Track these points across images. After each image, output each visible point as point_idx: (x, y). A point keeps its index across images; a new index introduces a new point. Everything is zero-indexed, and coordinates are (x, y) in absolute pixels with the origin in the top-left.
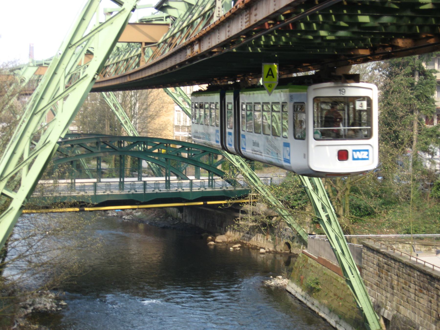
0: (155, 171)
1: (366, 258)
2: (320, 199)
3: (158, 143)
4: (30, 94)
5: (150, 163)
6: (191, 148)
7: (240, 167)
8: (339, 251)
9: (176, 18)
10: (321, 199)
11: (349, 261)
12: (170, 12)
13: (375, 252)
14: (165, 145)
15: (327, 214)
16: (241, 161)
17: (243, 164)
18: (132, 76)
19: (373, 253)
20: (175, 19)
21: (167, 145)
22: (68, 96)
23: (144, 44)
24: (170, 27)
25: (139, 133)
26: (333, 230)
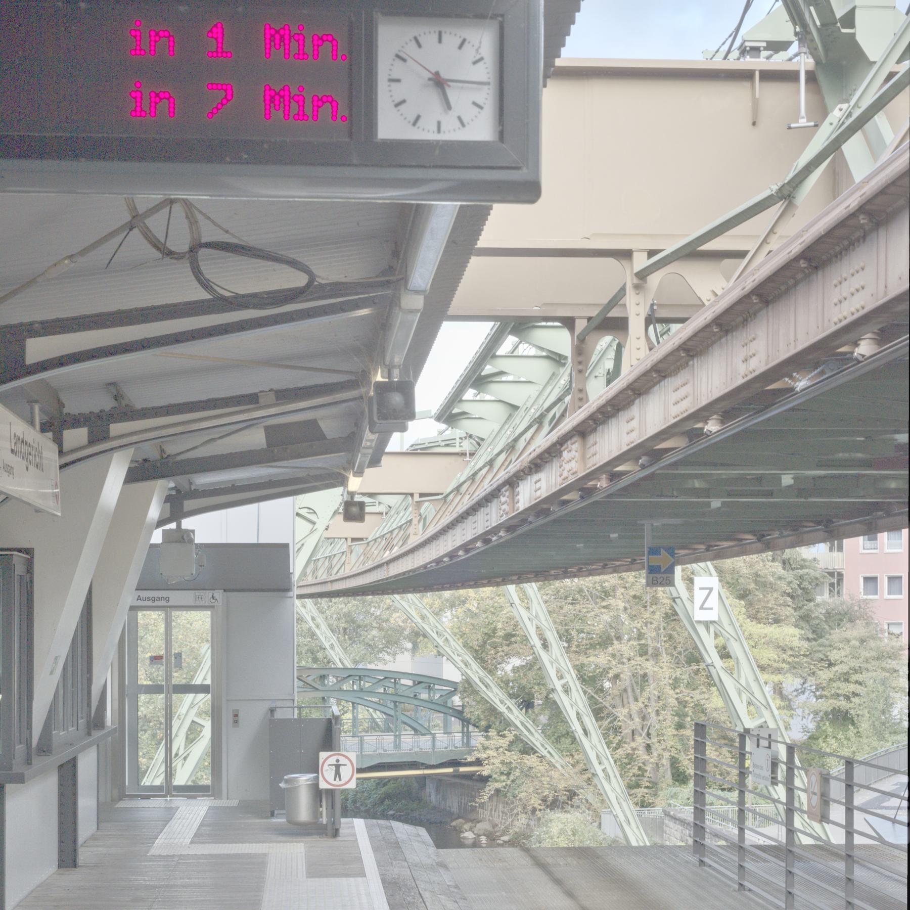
0: (380, 723)
1: (668, 832)
2: (593, 747)
3: (382, 678)
4: (754, 617)
5: (371, 710)
6: (434, 684)
7: (506, 711)
8: (622, 818)
9: (483, 440)
10: (595, 747)
11: (636, 831)
12: (467, 426)
13: (678, 822)
14: (393, 681)
15: (604, 767)
16: (507, 702)
17: (512, 707)
18: (391, 566)
19: (675, 823)
20: (480, 442)
21: (395, 680)
22: (751, 846)
23: (349, 540)
24: (468, 459)
25: (356, 662)
26: (614, 790)
